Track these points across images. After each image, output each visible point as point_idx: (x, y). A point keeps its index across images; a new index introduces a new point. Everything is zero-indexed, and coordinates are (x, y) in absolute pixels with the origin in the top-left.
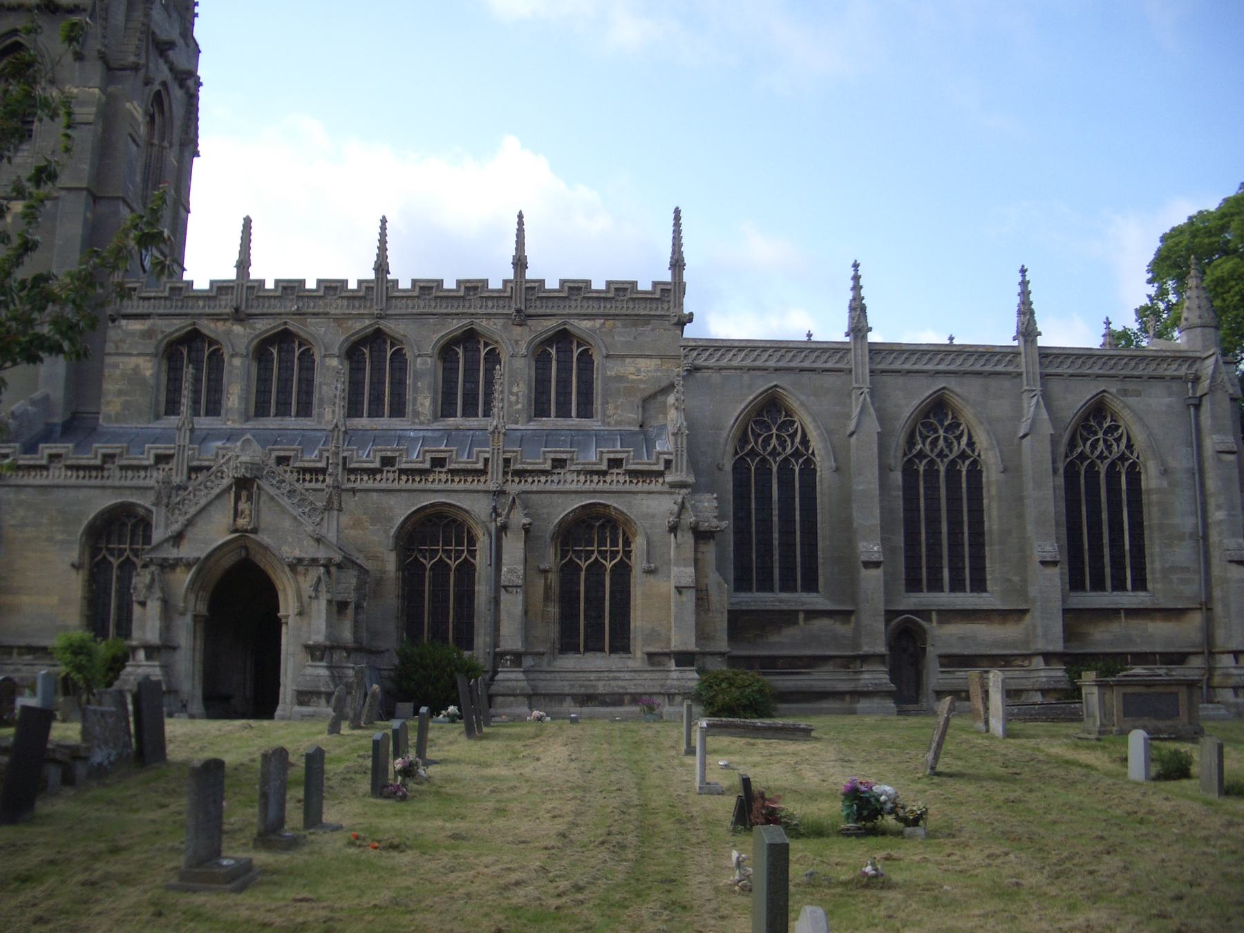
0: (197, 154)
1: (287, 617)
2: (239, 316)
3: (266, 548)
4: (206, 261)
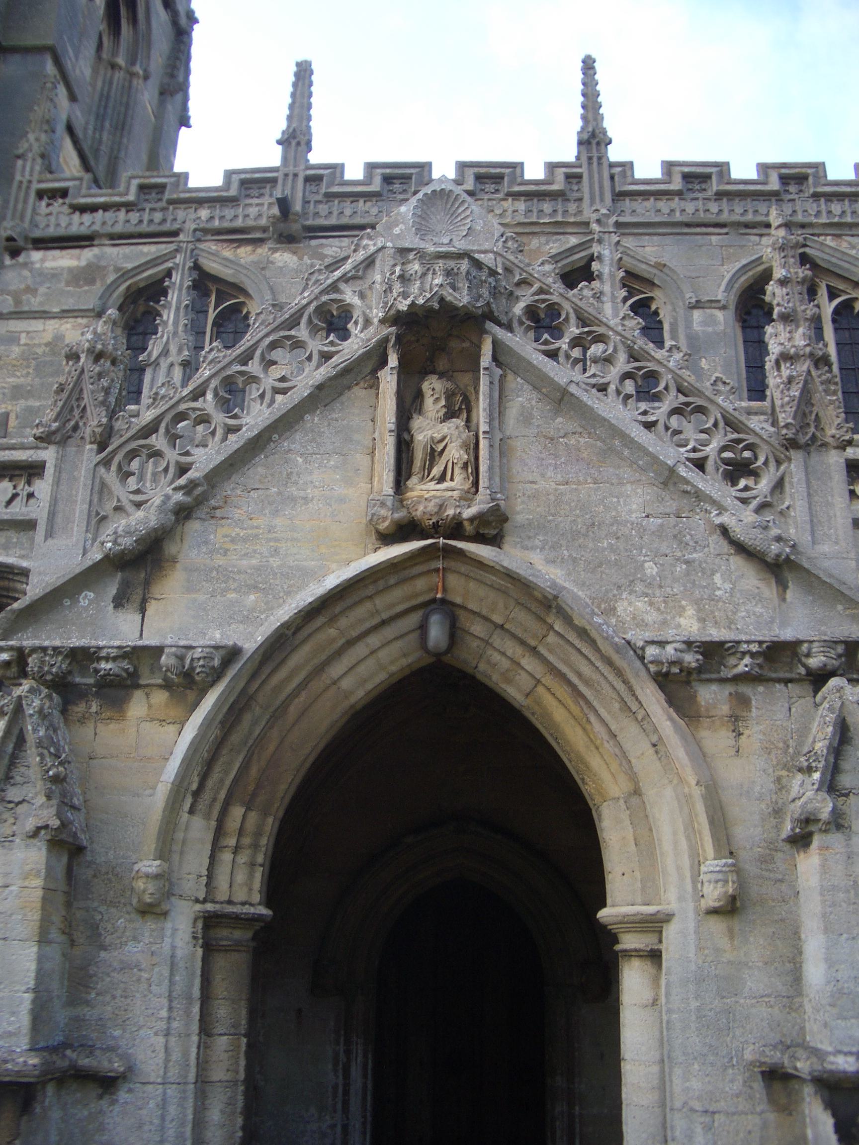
0: (185, 121)
1: (655, 924)
2: (290, 229)
3: (547, 605)
4: (221, 138)
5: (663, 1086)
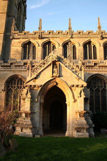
0: (26, 19)
5: (70, 113)
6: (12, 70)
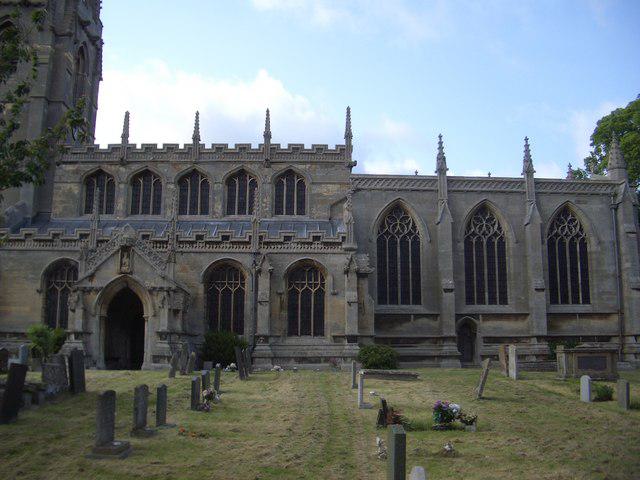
0: (101, 79)
4: (106, 135)
6: (56, 248)
